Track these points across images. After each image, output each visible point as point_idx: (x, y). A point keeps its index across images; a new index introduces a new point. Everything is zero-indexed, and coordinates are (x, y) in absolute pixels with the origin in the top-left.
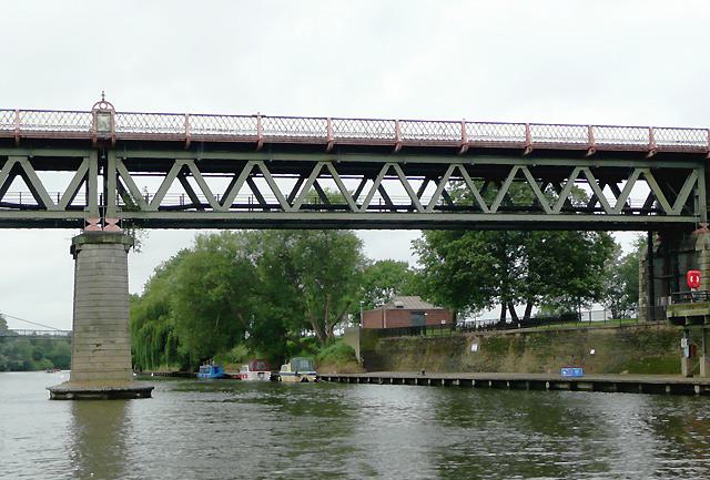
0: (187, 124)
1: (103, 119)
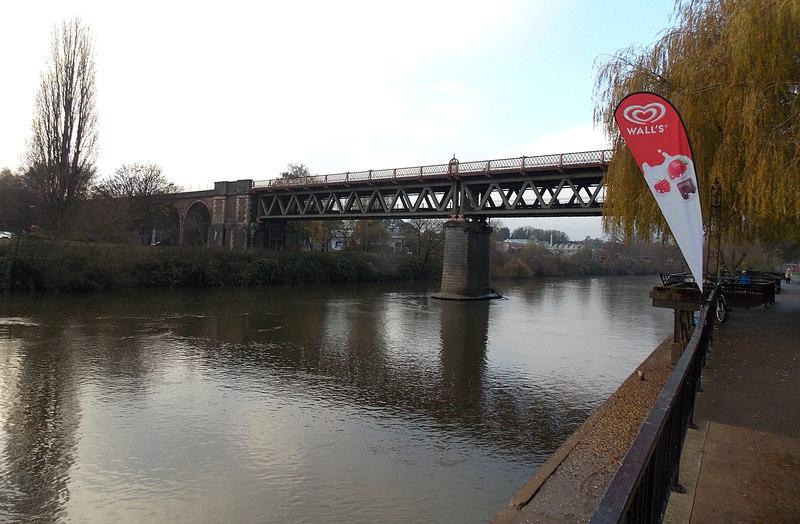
0: (562, 159)
1: (453, 167)
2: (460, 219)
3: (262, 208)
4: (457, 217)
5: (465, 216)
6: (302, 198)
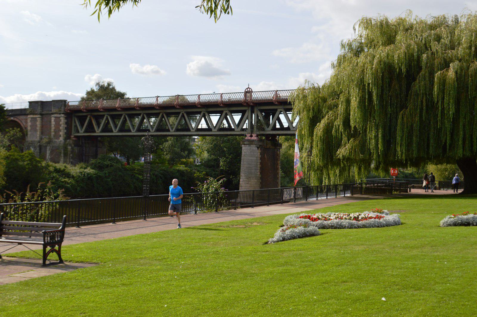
2: (254, 138)
3: (76, 126)
4: (251, 136)
5: (257, 136)
6: (98, 118)
